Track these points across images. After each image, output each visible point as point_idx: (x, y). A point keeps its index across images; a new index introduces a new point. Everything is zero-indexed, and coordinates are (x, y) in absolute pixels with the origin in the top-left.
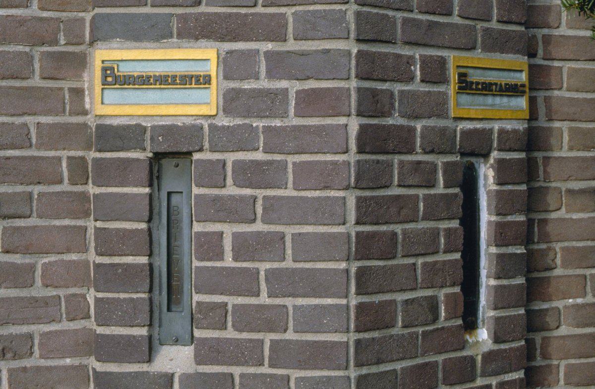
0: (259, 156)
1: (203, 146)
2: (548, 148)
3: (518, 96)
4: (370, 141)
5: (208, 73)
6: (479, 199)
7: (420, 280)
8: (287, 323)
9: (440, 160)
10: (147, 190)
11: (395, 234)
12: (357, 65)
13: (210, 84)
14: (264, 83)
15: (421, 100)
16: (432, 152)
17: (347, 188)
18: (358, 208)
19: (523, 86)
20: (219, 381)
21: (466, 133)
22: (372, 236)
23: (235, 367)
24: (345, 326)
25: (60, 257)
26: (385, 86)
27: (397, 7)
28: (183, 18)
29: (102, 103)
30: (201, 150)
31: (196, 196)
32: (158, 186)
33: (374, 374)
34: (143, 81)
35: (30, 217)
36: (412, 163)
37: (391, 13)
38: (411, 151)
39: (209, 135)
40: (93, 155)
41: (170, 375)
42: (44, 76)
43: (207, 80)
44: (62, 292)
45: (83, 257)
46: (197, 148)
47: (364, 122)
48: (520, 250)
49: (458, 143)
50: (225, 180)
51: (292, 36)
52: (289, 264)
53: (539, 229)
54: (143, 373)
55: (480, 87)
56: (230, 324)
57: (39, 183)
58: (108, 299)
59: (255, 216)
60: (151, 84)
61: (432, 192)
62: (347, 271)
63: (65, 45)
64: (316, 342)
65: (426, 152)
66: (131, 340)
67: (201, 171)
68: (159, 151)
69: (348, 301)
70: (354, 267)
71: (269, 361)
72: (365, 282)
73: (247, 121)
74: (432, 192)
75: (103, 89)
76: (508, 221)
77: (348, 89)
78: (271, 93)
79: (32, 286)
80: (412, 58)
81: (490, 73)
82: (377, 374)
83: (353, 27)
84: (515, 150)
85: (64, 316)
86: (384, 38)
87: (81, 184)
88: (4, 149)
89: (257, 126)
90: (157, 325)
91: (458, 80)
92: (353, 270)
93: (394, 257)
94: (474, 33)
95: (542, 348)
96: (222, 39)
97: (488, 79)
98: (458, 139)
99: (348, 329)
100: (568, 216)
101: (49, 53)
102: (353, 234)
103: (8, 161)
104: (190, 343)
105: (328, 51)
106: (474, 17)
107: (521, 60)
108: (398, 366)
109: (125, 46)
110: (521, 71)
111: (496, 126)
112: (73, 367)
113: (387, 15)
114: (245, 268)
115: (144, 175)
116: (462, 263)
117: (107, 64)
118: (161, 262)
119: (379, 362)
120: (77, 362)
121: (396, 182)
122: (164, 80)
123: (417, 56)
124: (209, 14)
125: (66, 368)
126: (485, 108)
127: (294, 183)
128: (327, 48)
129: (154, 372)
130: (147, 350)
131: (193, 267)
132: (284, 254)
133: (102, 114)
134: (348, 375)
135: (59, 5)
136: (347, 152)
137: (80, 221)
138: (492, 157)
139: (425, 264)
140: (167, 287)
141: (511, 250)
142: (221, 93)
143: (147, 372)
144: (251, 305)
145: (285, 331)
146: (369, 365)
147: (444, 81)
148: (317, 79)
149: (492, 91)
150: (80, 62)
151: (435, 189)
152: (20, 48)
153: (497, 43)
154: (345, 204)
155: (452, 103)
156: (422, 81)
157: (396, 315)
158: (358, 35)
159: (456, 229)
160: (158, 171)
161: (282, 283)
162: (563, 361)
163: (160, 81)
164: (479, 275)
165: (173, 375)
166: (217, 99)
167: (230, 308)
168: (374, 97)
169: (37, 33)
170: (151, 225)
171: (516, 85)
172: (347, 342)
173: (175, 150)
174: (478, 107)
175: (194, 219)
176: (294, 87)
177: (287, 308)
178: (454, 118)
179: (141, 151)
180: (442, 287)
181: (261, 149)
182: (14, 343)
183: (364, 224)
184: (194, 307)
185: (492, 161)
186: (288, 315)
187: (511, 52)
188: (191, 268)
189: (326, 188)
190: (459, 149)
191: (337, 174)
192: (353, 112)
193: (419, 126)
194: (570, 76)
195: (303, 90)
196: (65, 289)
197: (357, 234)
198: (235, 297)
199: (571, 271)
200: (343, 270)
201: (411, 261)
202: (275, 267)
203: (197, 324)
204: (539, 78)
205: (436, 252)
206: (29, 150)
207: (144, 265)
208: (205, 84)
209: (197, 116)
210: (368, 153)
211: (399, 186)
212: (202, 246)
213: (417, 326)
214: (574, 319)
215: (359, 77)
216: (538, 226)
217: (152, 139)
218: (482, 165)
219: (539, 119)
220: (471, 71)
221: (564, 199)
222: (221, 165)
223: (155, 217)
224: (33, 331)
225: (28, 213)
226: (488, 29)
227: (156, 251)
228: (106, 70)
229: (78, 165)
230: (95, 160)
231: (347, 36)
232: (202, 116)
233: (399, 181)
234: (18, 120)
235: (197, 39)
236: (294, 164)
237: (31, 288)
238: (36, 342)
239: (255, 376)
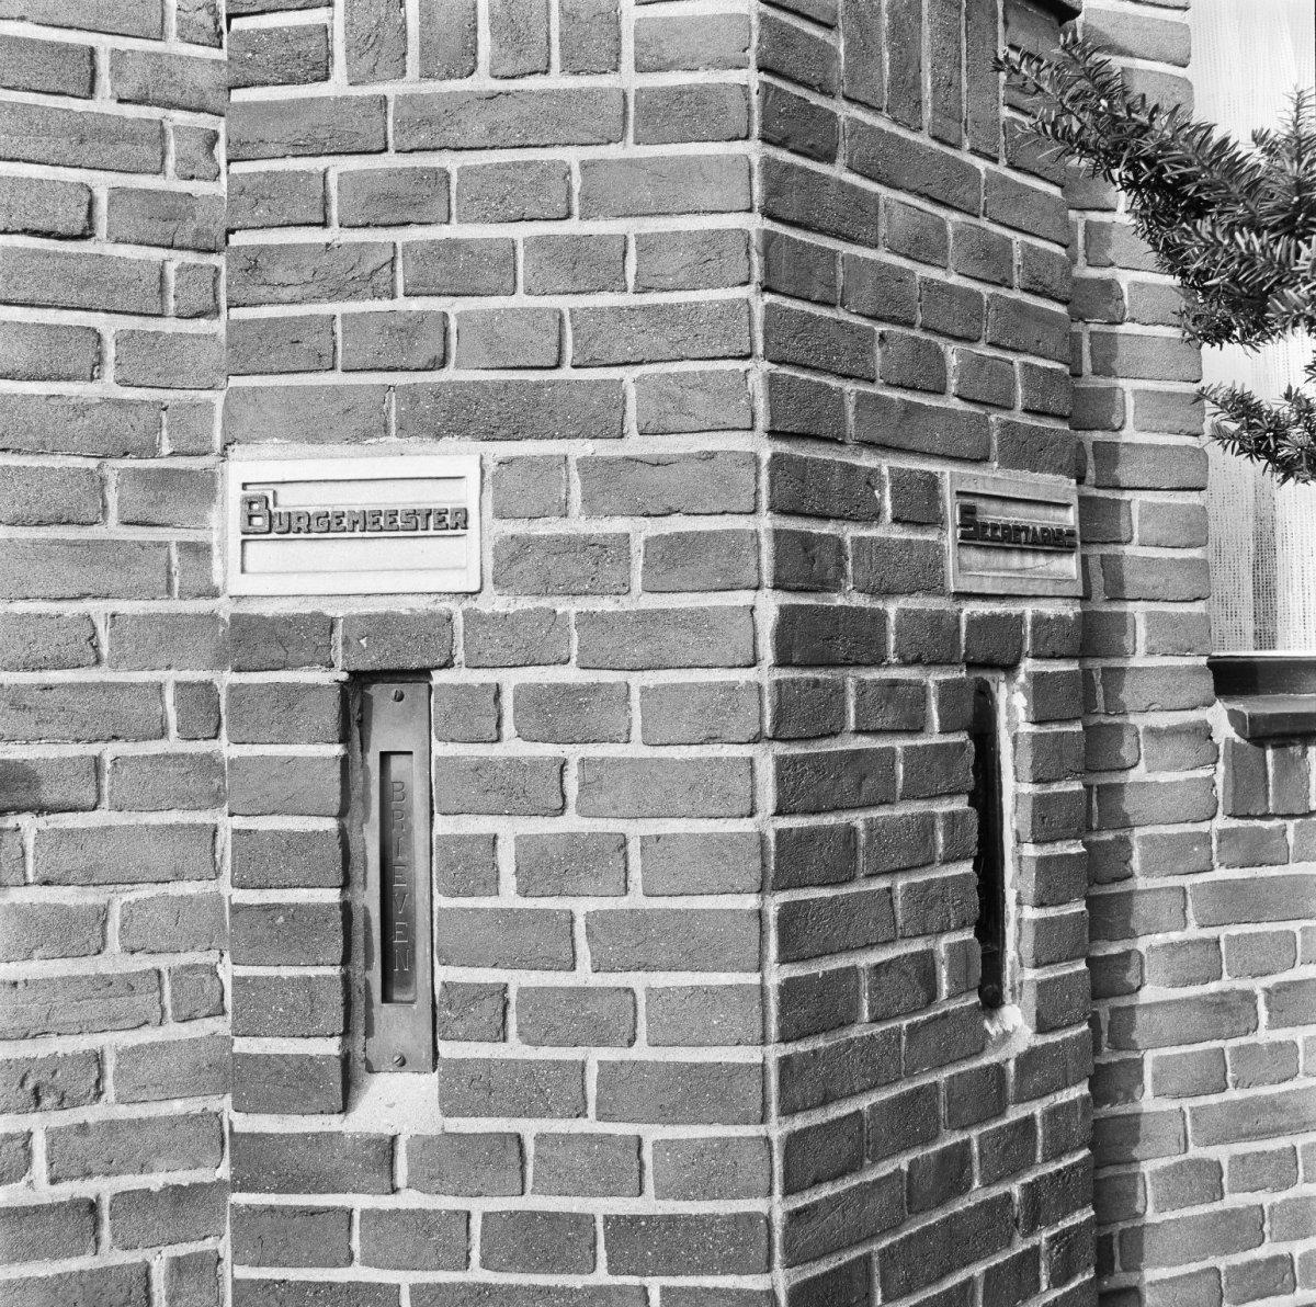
0: (570, 675)
1: (452, 657)
2: (1122, 653)
3: (1062, 553)
4: (802, 640)
5: (462, 506)
6: (999, 753)
7: (900, 922)
8: (635, 1026)
9: (933, 678)
10: (338, 750)
11: (851, 831)
12: (772, 484)
13: (466, 528)
14: (579, 525)
15: (895, 558)
16: (917, 661)
17: (756, 740)
18: (780, 780)
19: (1071, 534)
20: (491, 1152)
21: (976, 624)
22: (810, 835)
23: (526, 1120)
24: (758, 1033)
25: (160, 889)
26: (828, 528)
27: (845, 370)
28: (411, 395)
29: (243, 571)
30: (448, 665)
31: (439, 759)
32: (361, 740)
33: (818, 1127)
35: (95, 808)
36: (880, 683)
37: (834, 383)
38: (878, 661)
39: (465, 633)
40: (227, 678)
41: (388, 1140)
42: (127, 518)
43: (461, 520)
44: (163, 962)
45: (210, 887)
46: (441, 660)
47: (787, 602)
48: (1076, 848)
49: (963, 644)
50: (498, 726)
51: (634, 426)
52: (636, 900)
53: (1099, 805)
54: (331, 1135)
55: (999, 534)
56: (512, 1029)
57: (115, 738)
58: (255, 978)
59: (564, 801)
60: (344, 530)
61: (920, 742)
62: (760, 914)
63: (172, 454)
64: (696, 1066)
65: (906, 663)
66: (306, 1067)
67: (448, 708)
68: (361, 667)
69: (763, 978)
70: (774, 903)
71: (598, 1107)
72: (796, 934)
73: (545, 603)
74: (920, 742)
75: (244, 542)
76: (1055, 794)
77: (755, 534)
79: (99, 952)
80: (874, 472)
81: (1014, 508)
82: (824, 1125)
83: (761, 406)
84: (1061, 657)
85: (169, 1012)
86: (823, 432)
87: (205, 739)
88: (40, 668)
89: (565, 614)
90: (361, 1031)
91: (961, 519)
92: (772, 912)
93: (850, 880)
94: (985, 430)
95: (1110, 1030)
96: (489, 436)
97: (1011, 518)
98: (963, 636)
99: (764, 1037)
100: (1150, 778)
101: (137, 472)
102: (771, 836)
103: (48, 694)
104: (430, 1068)
105: (711, 455)
106: (984, 399)
107: (1066, 486)
108: (864, 1103)
109: (290, 453)
110: (1067, 506)
111: (1028, 610)
112: (189, 1119)
113: (827, 386)
114: (543, 911)
115: (329, 717)
116: (975, 880)
117: (252, 491)
118: (369, 898)
119: (826, 1101)
120: (196, 1106)
121: (852, 725)
122: (373, 523)
123: (885, 471)
124: (462, 385)
125: (172, 1122)
126: (1008, 574)
127: (644, 731)
128: (709, 449)
129: (353, 1135)
130: (339, 1087)
131: (435, 909)
132: (626, 881)
133: (243, 593)
134: (764, 1134)
135: (159, 375)
136: (754, 665)
137: (202, 814)
138: (1022, 670)
139: (909, 888)
140: (381, 949)
141: (1061, 848)
142: (489, 545)
143: (339, 1133)
144: (556, 989)
145: (631, 1043)
146: (809, 1108)
147: (936, 522)
148: (689, 514)
149: (1019, 542)
150: (205, 488)
151: (923, 735)
152: (78, 462)
153: (1024, 452)
154: (752, 771)
155: (950, 564)
156: (896, 520)
157: (858, 999)
158: (773, 422)
159: (965, 813)
160: (361, 710)
161: (630, 941)
162: (1149, 1051)
163: (362, 522)
164: (1004, 902)
165: (394, 1139)
167: (512, 995)
168: (806, 550)
169: (113, 431)
170: (347, 822)
171: (1060, 532)
172: (763, 1065)
173: (394, 665)
174: (995, 574)
175: (435, 809)
176: (642, 530)
177: (634, 995)
178: (955, 593)
179: (324, 668)
180: (942, 932)
181: (574, 660)
182: (59, 1074)
183: (792, 813)
184: (437, 993)
185: (1022, 678)
186: (635, 1010)
187: (1049, 471)
188: (432, 912)
189: (710, 740)
190: (965, 655)
191: (734, 710)
192: (767, 579)
193: (892, 608)
194: (1144, 519)
195: (660, 537)
196: (169, 956)
197: (780, 833)
198: (523, 972)
199: (1159, 880)
200: (750, 913)
201: (881, 884)
202: (607, 908)
203: (445, 1032)
204: (1100, 521)
205: (928, 863)
206: (94, 670)
207: (331, 907)
208: (456, 528)
210: (797, 665)
211: (858, 732)
212: (452, 866)
213: (898, 1015)
214: (1166, 972)
215: (778, 509)
216: (1098, 800)
217: (346, 642)
218: (1003, 686)
219: (1094, 596)
220: (981, 504)
221: (1142, 746)
222: (491, 697)
223: (356, 806)
224: (101, 1047)
225: (92, 801)
226: (1009, 423)
227: (357, 875)
228: (251, 503)
229: (200, 699)
230: (232, 689)
231: (748, 425)
233: (857, 721)
234: (71, 609)
235: (438, 436)
236: (644, 690)
237: (99, 957)
238: (110, 1068)
239: (568, 1138)
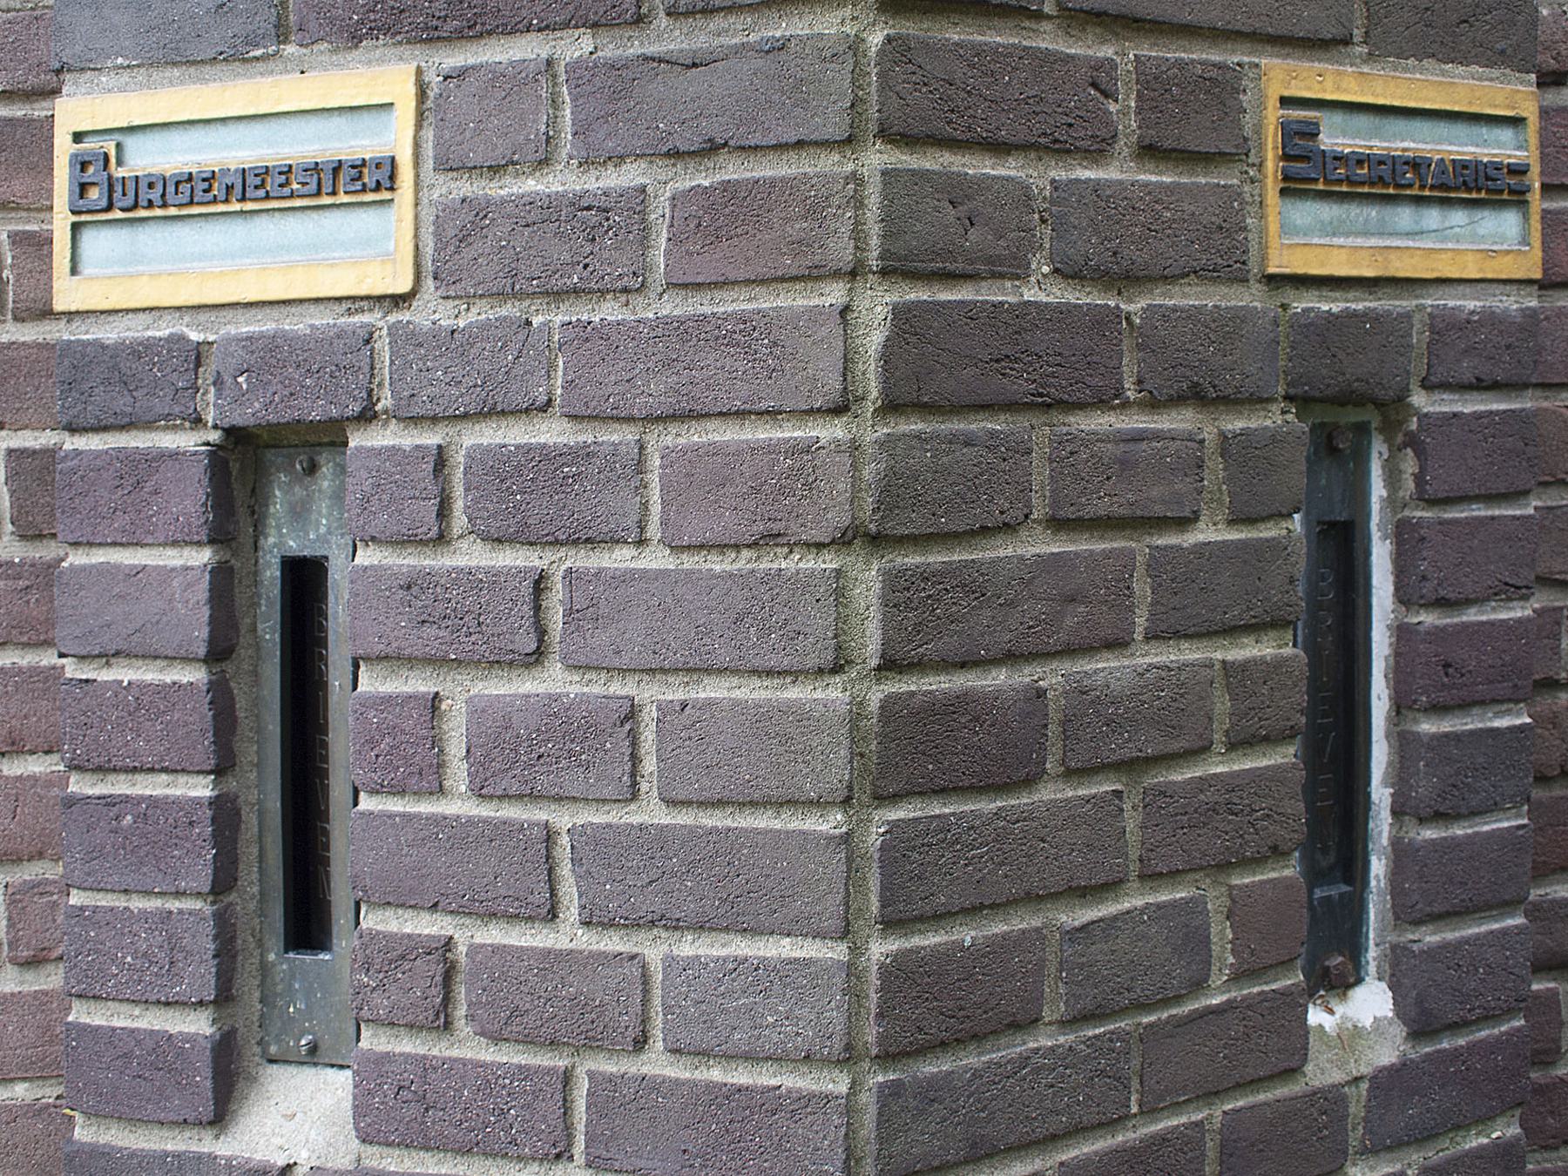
10: (202, 557)
30: (367, 416)
34: (195, 194)
46: (355, 408)
75: (76, 227)
78: (588, 208)
89: (546, 324)
93: (1029, 782)
96: (431, 36)
105: (781, 46)
122: (257, 189)
132: (633, 775)
142: (428, 216)
145: (640, 1043)
166: (416, 236)
209: (353, 299)
212: (372, 743)
232: (368, 298)
235: (355, 40)
